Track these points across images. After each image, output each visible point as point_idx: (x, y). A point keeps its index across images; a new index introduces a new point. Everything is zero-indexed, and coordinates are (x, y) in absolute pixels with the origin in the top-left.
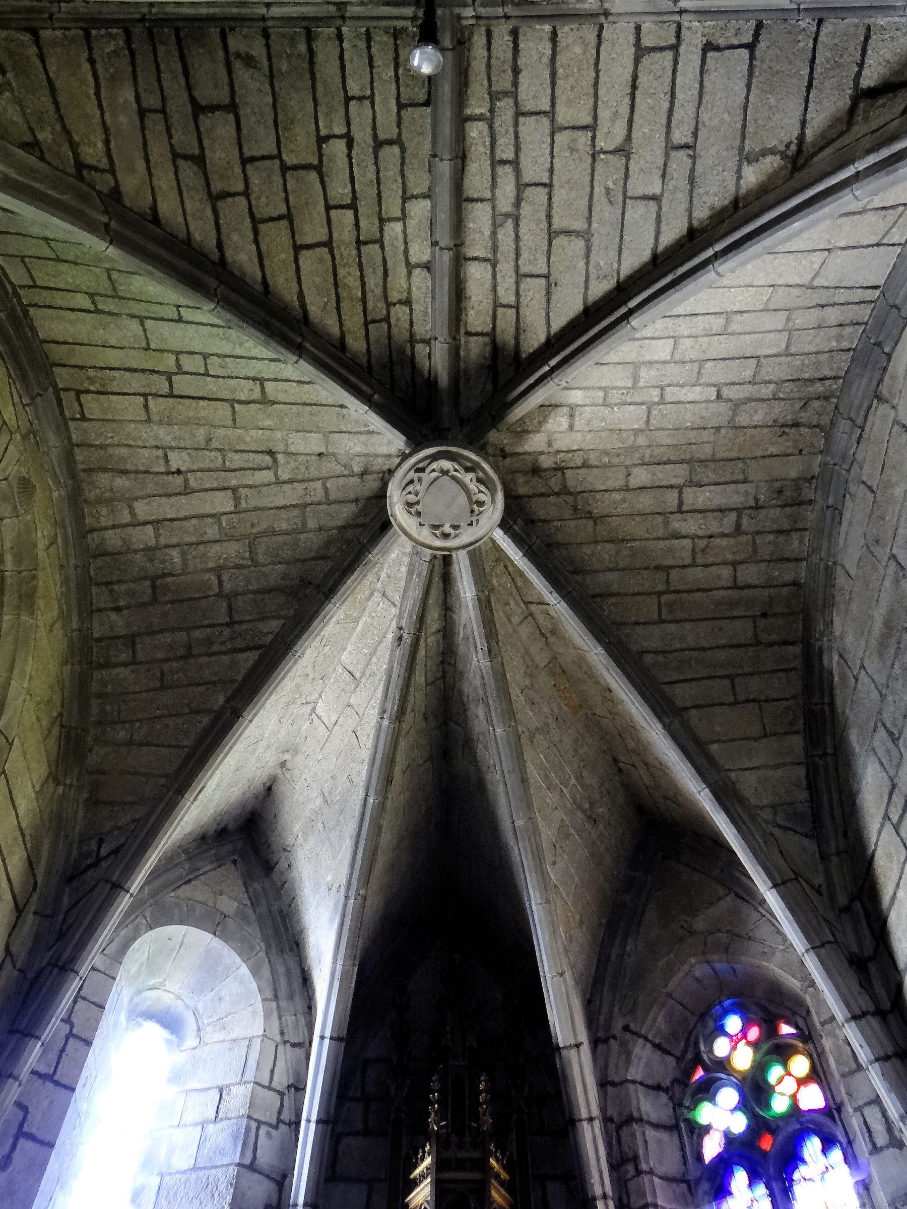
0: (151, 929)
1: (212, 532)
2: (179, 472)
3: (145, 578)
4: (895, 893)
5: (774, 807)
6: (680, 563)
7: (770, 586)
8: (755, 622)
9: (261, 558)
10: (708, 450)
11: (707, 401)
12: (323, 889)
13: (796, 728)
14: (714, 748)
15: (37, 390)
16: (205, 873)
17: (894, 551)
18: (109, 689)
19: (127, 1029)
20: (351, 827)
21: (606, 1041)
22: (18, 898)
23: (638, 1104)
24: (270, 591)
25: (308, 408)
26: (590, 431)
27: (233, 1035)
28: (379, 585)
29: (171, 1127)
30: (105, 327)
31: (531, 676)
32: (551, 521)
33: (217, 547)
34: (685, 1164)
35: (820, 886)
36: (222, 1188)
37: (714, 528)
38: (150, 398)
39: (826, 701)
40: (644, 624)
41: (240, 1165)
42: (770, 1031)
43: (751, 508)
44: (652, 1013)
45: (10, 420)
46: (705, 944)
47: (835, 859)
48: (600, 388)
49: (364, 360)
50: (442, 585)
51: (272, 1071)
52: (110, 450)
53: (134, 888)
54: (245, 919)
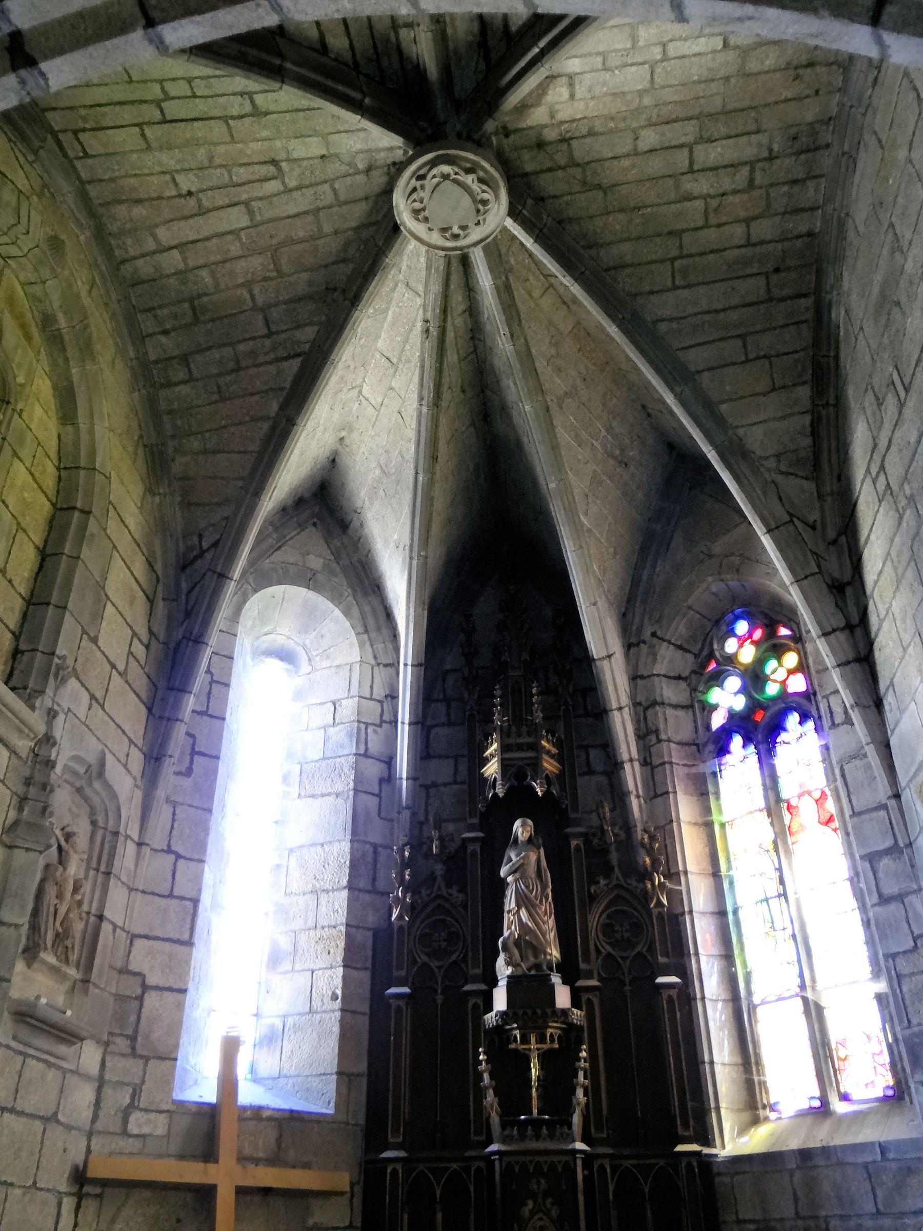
1: (235, 249)
2: (190, 193)
3: (183, 301)
4: (869, 535)
5: (778, 456)
6: (693, 225)
7: (782, 241)
8: (767, 278)
9: (285, 268)
10: (718, 102)
11: (714, 52)
12: (392, 545)
13: (804, 379)
14: (724, 408)
16: (292, 538)
17: (894, 219)
18: (176, 405)
19: (254, 665)
20: (408, 497)
21: (637, 645)
22: (148, 592)
23: (661, 692)
24: (300, 299)
25: (301, 114)
26: (592, 98)
27: (337, 662)
28: (401, 277)
29: (301, 731)
31: (556, 345)
32: (562, 196)
33: (242, 263)
34: (696, 732)
35: (815, 521)
36: (346, 770)
37: (727, 184)
38: (145, 127)
39: (832, 354)
40: (657, 292)
41: (356, 754)
42: (771, 631)
43: (765, 159)
44: (675, 622)
45: (24, 185)
46: (721, 566)
47: (829, 499)
48: (598, 54)
49: (348, 56)
50: (461, 268)
51: (372, 687)
52: (121, 182)
53: (236, 575)
54: (332, 572)
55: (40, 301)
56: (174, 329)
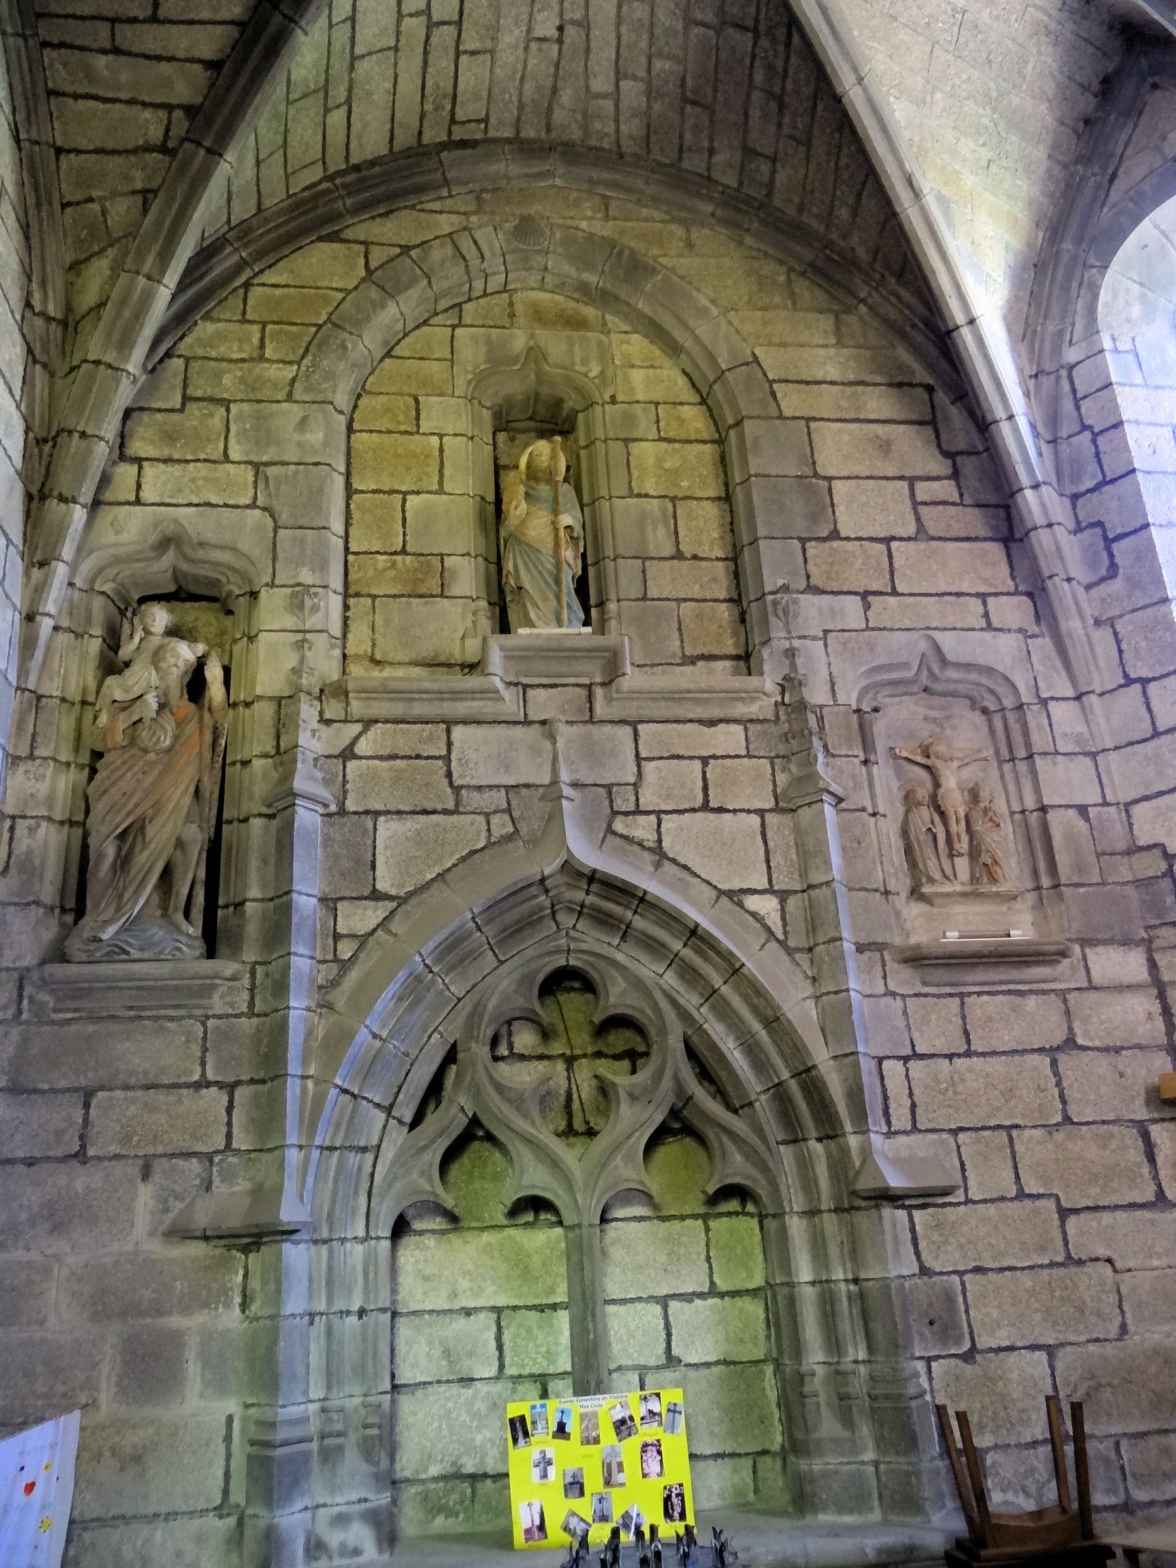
0: (1106, 267)
2: (561, 29)
3: (682, 110)
15: (438, 175)
18: (797, 199)
30: (369, 94)
33: (660, 12)
52: (526, 99)
55: (563, 284)
56: (712, 140)
